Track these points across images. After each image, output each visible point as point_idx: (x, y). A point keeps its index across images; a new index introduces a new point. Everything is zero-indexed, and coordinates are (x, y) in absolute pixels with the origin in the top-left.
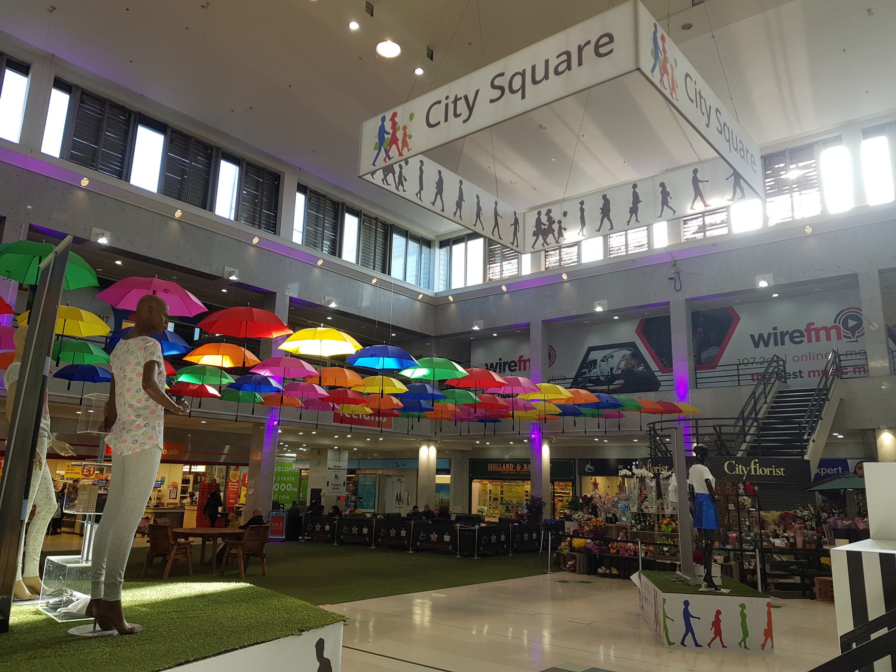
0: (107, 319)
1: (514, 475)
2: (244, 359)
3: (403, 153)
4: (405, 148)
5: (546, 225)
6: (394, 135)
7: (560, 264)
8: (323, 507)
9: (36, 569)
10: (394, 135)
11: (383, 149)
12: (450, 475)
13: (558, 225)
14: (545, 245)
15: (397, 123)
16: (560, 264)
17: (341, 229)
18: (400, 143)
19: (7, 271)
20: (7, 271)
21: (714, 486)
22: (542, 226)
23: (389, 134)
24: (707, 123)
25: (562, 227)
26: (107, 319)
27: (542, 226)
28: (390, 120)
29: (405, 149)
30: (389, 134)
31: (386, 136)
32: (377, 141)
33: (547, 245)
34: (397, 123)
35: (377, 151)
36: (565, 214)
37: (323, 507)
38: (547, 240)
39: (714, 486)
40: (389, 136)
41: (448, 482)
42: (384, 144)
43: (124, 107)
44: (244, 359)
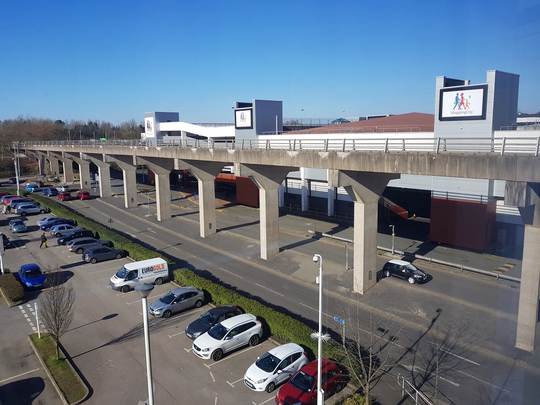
3: (466, 108)
6: (462, 101)
9: (228, 360)
10: (462, 101)
11: (457, 104)
12: (430, 218)
14: (459, 109)
15: (464, 97)
19: (55, 172)
20: (55, 172)
21: (228, 203)
23: (460, 100)
28: (461, 95)
29: (467, 108)
30: (460, 100)
31: (459, 101)
32: (455, 101)
33: (461, 109)
34: (464, 97)
35: (455, 105)
36: (470, 97)
38: (461, 107)
39: (228, 203)
40: (461, 101)
41: (429, 222)
42: (458, 103)
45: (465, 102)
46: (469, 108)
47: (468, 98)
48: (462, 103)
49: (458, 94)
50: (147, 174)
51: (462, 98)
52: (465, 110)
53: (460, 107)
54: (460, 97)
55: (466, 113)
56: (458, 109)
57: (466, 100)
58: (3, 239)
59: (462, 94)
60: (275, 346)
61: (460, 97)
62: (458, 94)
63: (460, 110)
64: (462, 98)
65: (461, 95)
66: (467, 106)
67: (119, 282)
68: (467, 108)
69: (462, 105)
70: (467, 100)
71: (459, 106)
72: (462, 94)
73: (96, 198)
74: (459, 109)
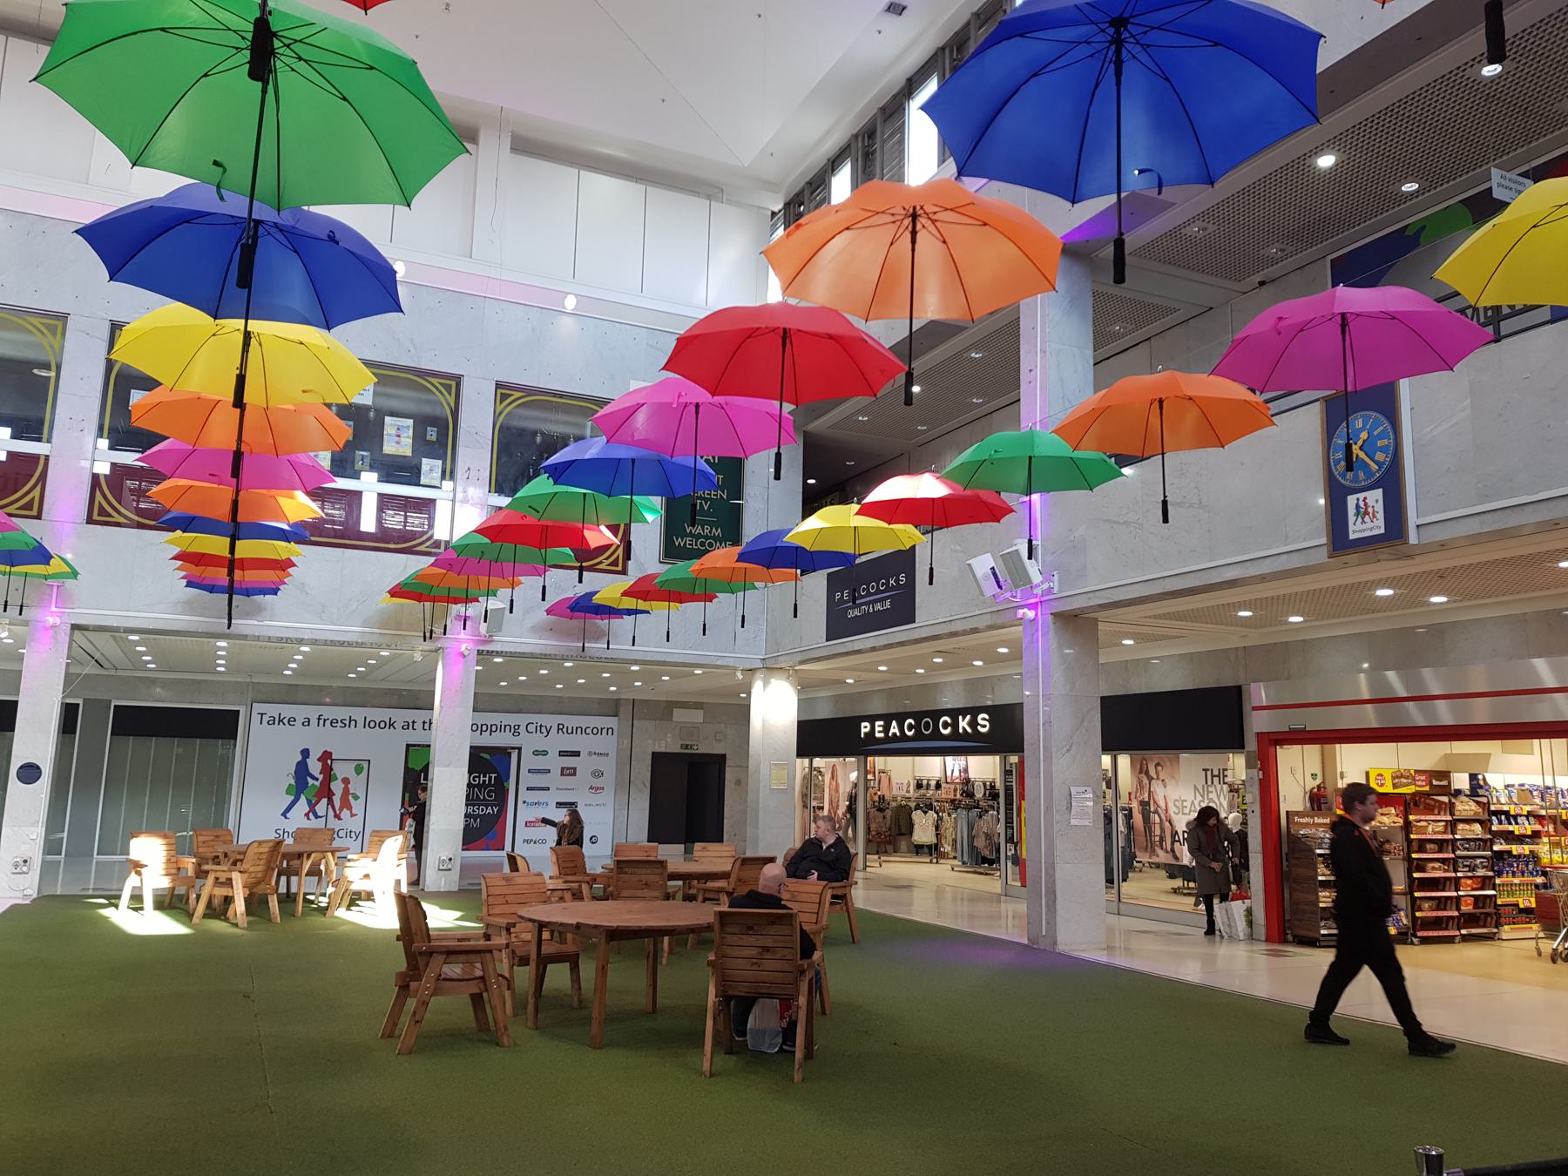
0: (899, 830)
1: (337, 534)
2: (931, 564)
4: (345, 810)
5: (317, 779)
7: (406, 513)
8: (358, 478)
11: (303, 797)
13: (343, 786)
14: (311, 815)
16: (406, 513)
17: (452, 460)
18: (337, 800)
22: (309, 779)
24: (1023, 802)
25: (351, 792)
26: (899, 830)
27: (309, 779)
28: (319, 760)
31: (311, 781)
37: (358, 478)
38: (317, 808)
40: (317, 784)
43: (426, 919)
44: (931, 564)
45: (1370, 510)
46: (352, 815)
47: (351, 775)
48: (1366, 513)
49: (1358, 499)
50: (1320, 890)
51: (1366, 504)
52: (1371, 525)
53: (1363, 521)
54: (315, 767)
55: (335, 836)
56: (307, 815)
57: (340, 778)
58: (434, 691)
59: (1365, 498)
60: (1094, 4)
61: (315, 767)
62: (1358, 499)
63: (1365, 526)
64: (1366, 504)
65: (319, 760)
66: (1374, 516)
67: (780, 292)
68: (1375, 520)
69: (1367, 516)
70: (346, 781)
71: (309, 802)
72: (1365, 498)
73: (31, 901)
74: (311, 815)
